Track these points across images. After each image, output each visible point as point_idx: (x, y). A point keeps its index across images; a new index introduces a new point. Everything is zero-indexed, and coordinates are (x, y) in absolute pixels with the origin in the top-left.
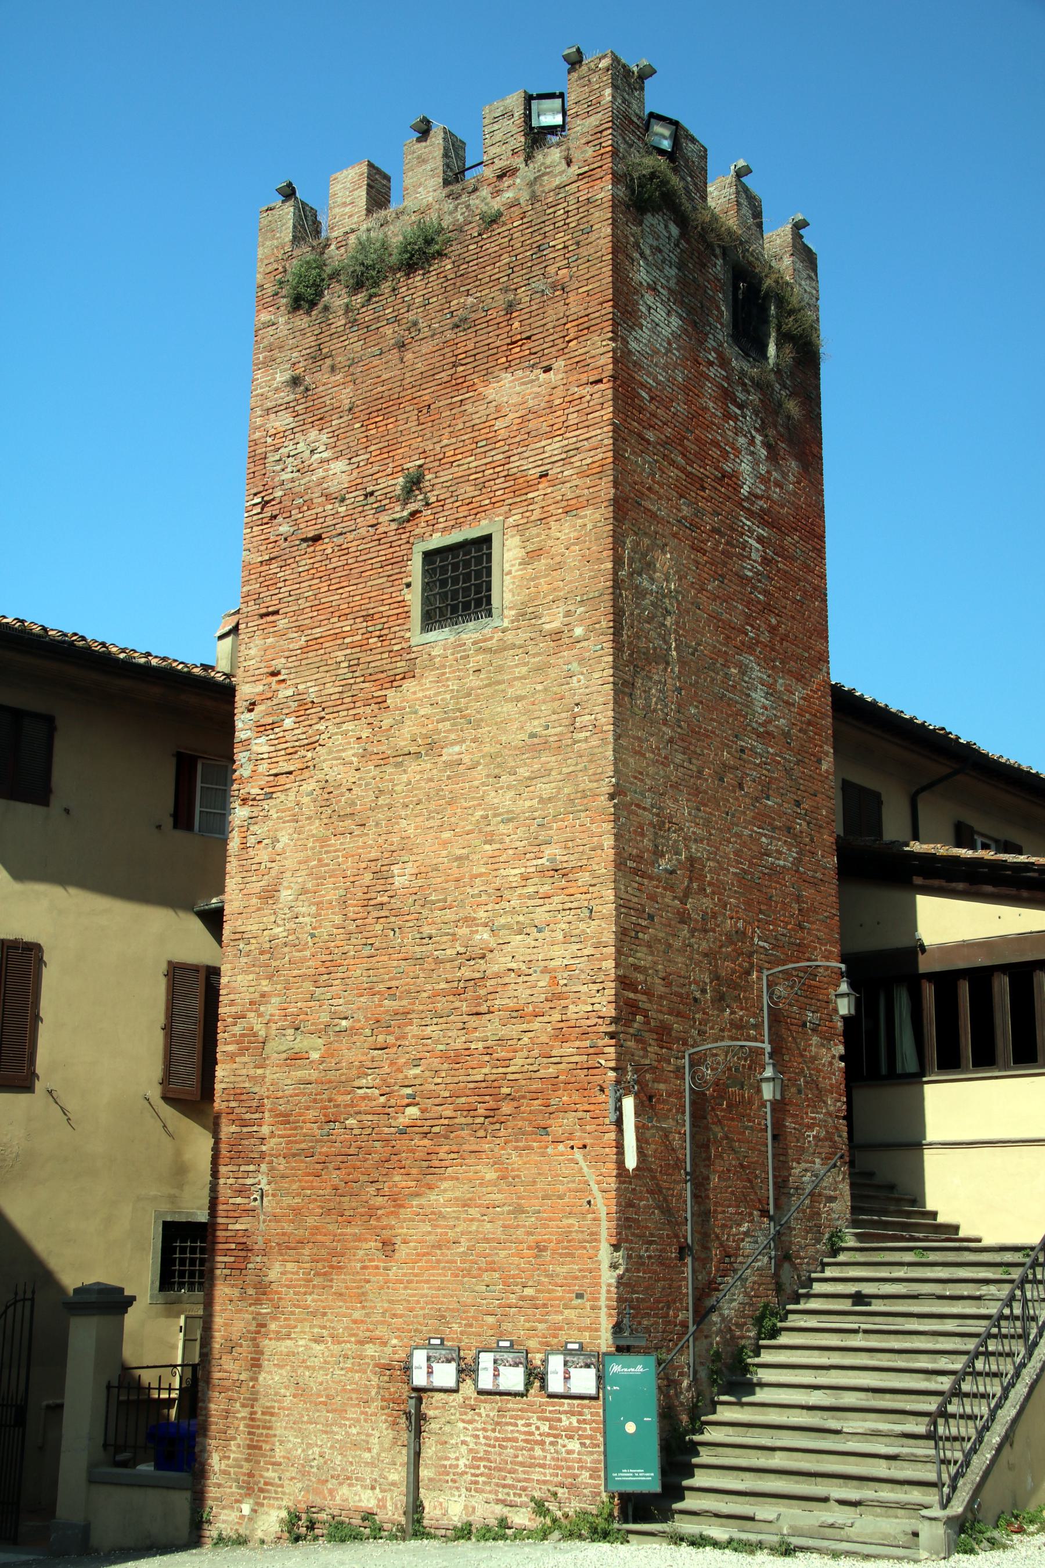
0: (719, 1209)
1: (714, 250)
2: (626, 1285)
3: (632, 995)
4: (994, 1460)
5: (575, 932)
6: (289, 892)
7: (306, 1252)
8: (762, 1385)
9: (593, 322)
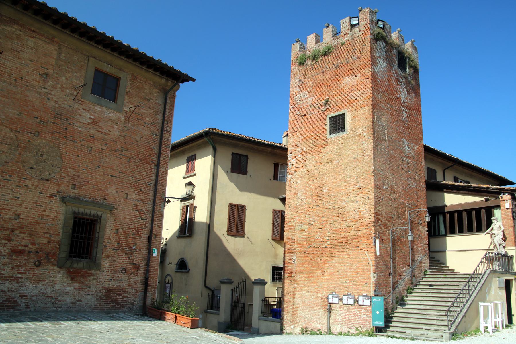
4: (461, 321)
8: (408, 304)
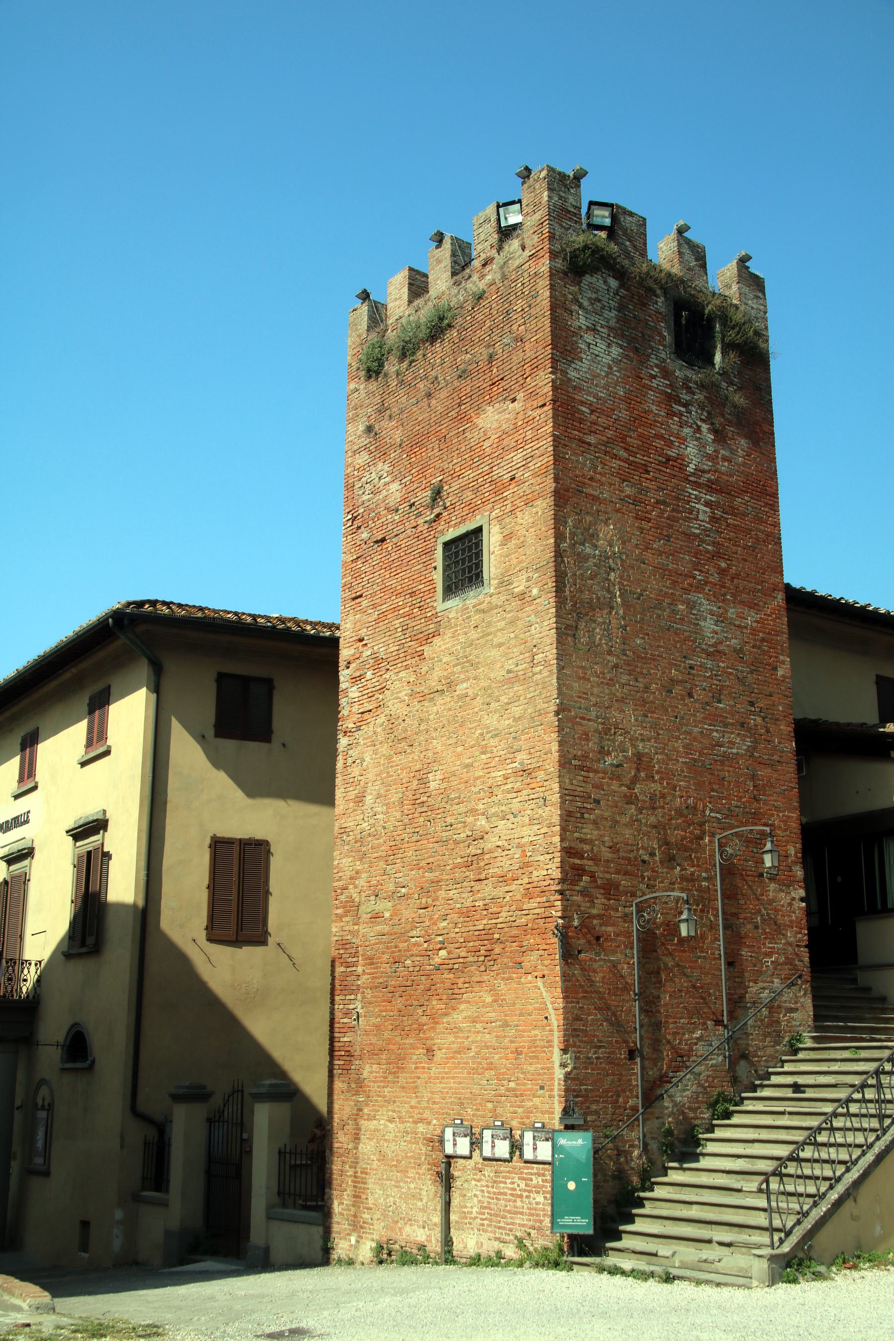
0: (671, 1020)
1: (655, 292)
2: (573, 1079)
3: (577, 861)
5: (536, 816)
6: (371, 797)
7: (384, 1057)
9: (540, 362)
